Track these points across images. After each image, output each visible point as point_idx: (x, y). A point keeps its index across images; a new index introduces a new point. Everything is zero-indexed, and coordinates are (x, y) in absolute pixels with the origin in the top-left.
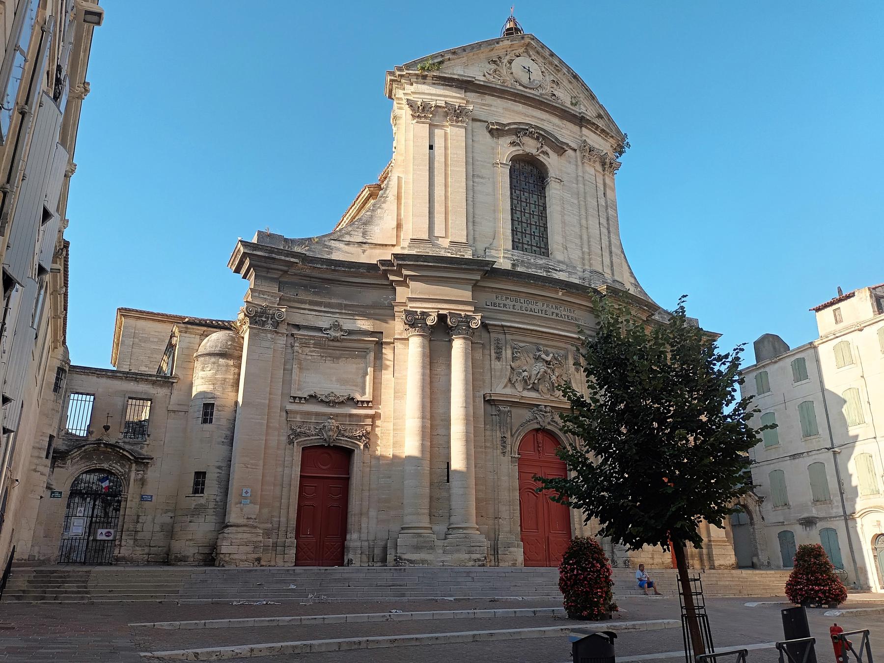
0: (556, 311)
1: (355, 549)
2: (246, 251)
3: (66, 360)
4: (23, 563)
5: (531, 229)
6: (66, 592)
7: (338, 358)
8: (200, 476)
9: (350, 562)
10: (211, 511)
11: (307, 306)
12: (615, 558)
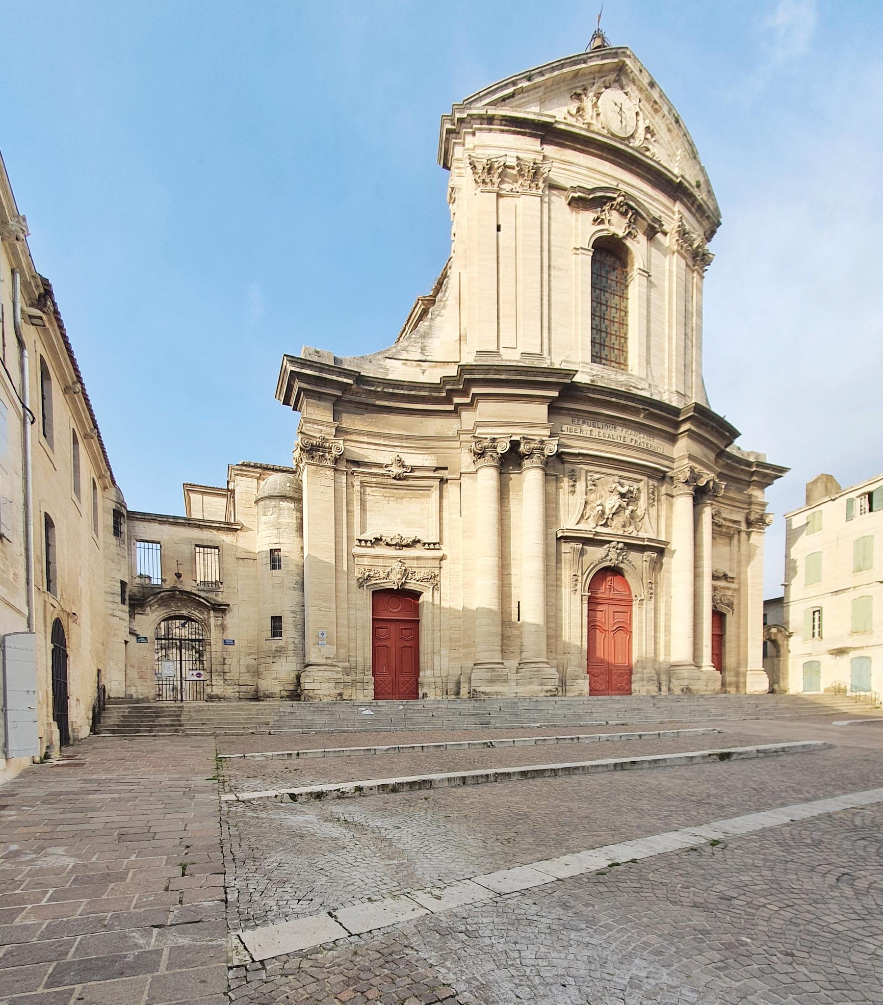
0: (635, 438)
1: (429, 684)
2: (293, 369)
3: (121, 503)
4: (118, 701)
5: (606, 341)
6: (160, 726)
7: (402, 498)
8: (276, 621)
9: (425, 695)
10: (291, 653)
11: (365, 439)
12: (672, 686)
